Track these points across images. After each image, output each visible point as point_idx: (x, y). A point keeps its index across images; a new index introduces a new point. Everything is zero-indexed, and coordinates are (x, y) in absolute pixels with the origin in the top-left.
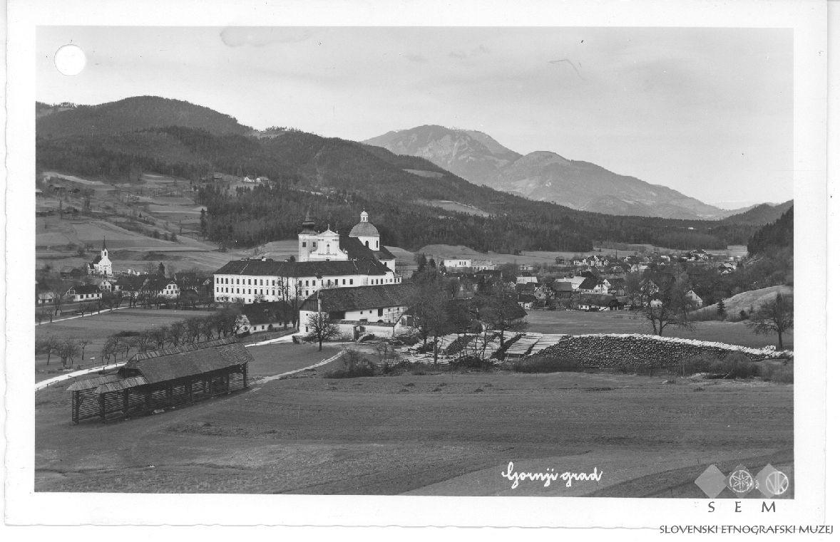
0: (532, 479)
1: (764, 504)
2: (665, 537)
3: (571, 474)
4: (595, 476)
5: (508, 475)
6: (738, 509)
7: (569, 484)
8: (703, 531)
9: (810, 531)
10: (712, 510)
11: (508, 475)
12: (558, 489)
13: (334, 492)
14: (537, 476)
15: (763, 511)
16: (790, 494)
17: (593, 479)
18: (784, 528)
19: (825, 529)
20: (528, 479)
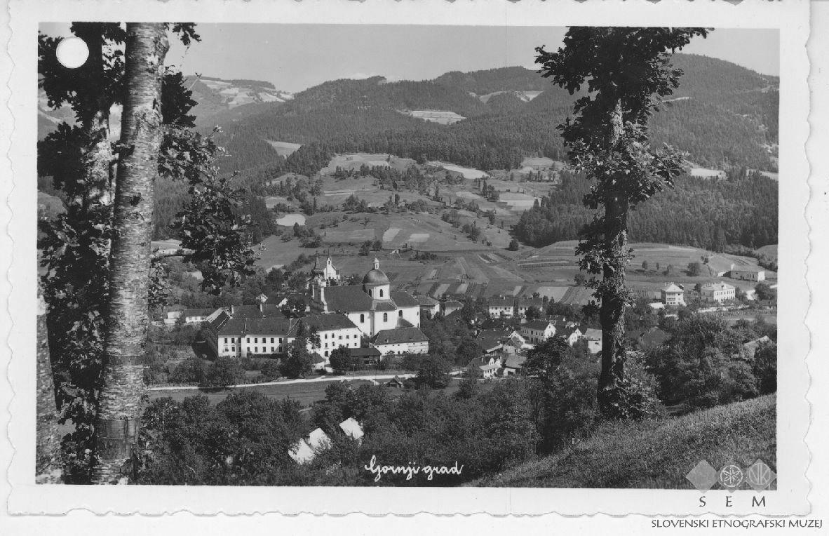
0: (394, 472)
1: (754, 498)
2: (657, 531)
3: (432, 468)
4: (455, 470)
5: (371, 468)
6: (729, 504)
7: (430, 478)
8: (694, 525)
9: (799, 525)
10: (703, 504)
11: (371, 468)
12: (420, 481)
13: (483, 469)
14: (399, 470)
15: (753, 506)
16: (773, 485)
17: (453, 472)
18: (774, 523)
19: (816, 523)
20: (390, 472)
